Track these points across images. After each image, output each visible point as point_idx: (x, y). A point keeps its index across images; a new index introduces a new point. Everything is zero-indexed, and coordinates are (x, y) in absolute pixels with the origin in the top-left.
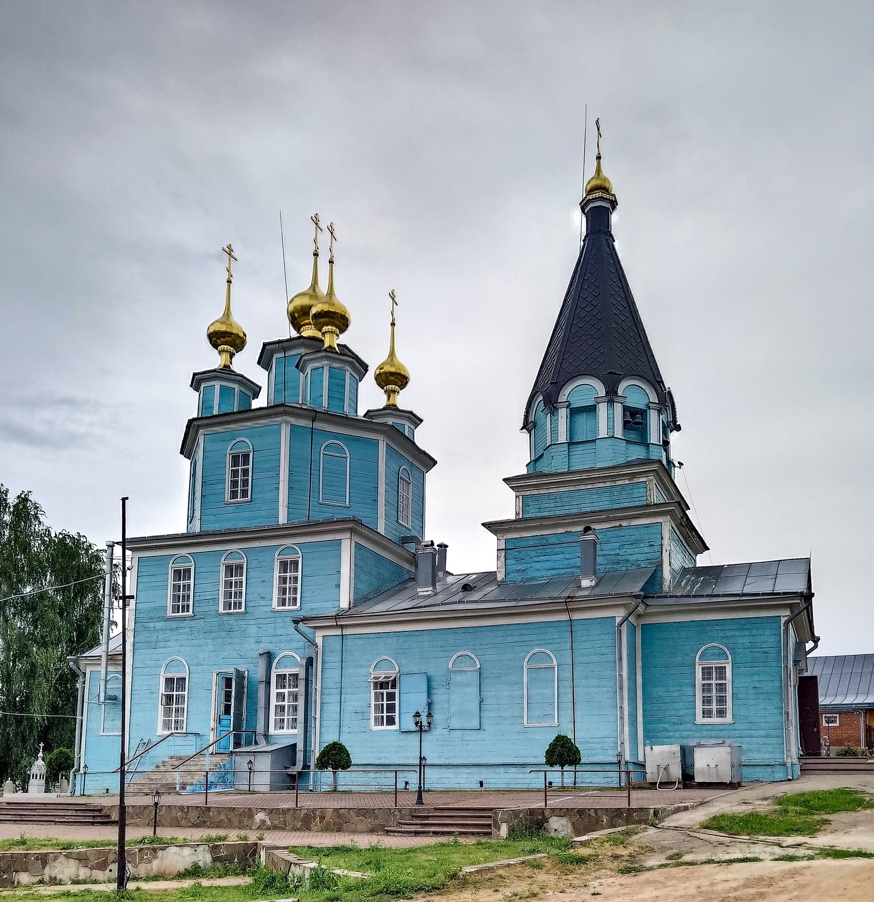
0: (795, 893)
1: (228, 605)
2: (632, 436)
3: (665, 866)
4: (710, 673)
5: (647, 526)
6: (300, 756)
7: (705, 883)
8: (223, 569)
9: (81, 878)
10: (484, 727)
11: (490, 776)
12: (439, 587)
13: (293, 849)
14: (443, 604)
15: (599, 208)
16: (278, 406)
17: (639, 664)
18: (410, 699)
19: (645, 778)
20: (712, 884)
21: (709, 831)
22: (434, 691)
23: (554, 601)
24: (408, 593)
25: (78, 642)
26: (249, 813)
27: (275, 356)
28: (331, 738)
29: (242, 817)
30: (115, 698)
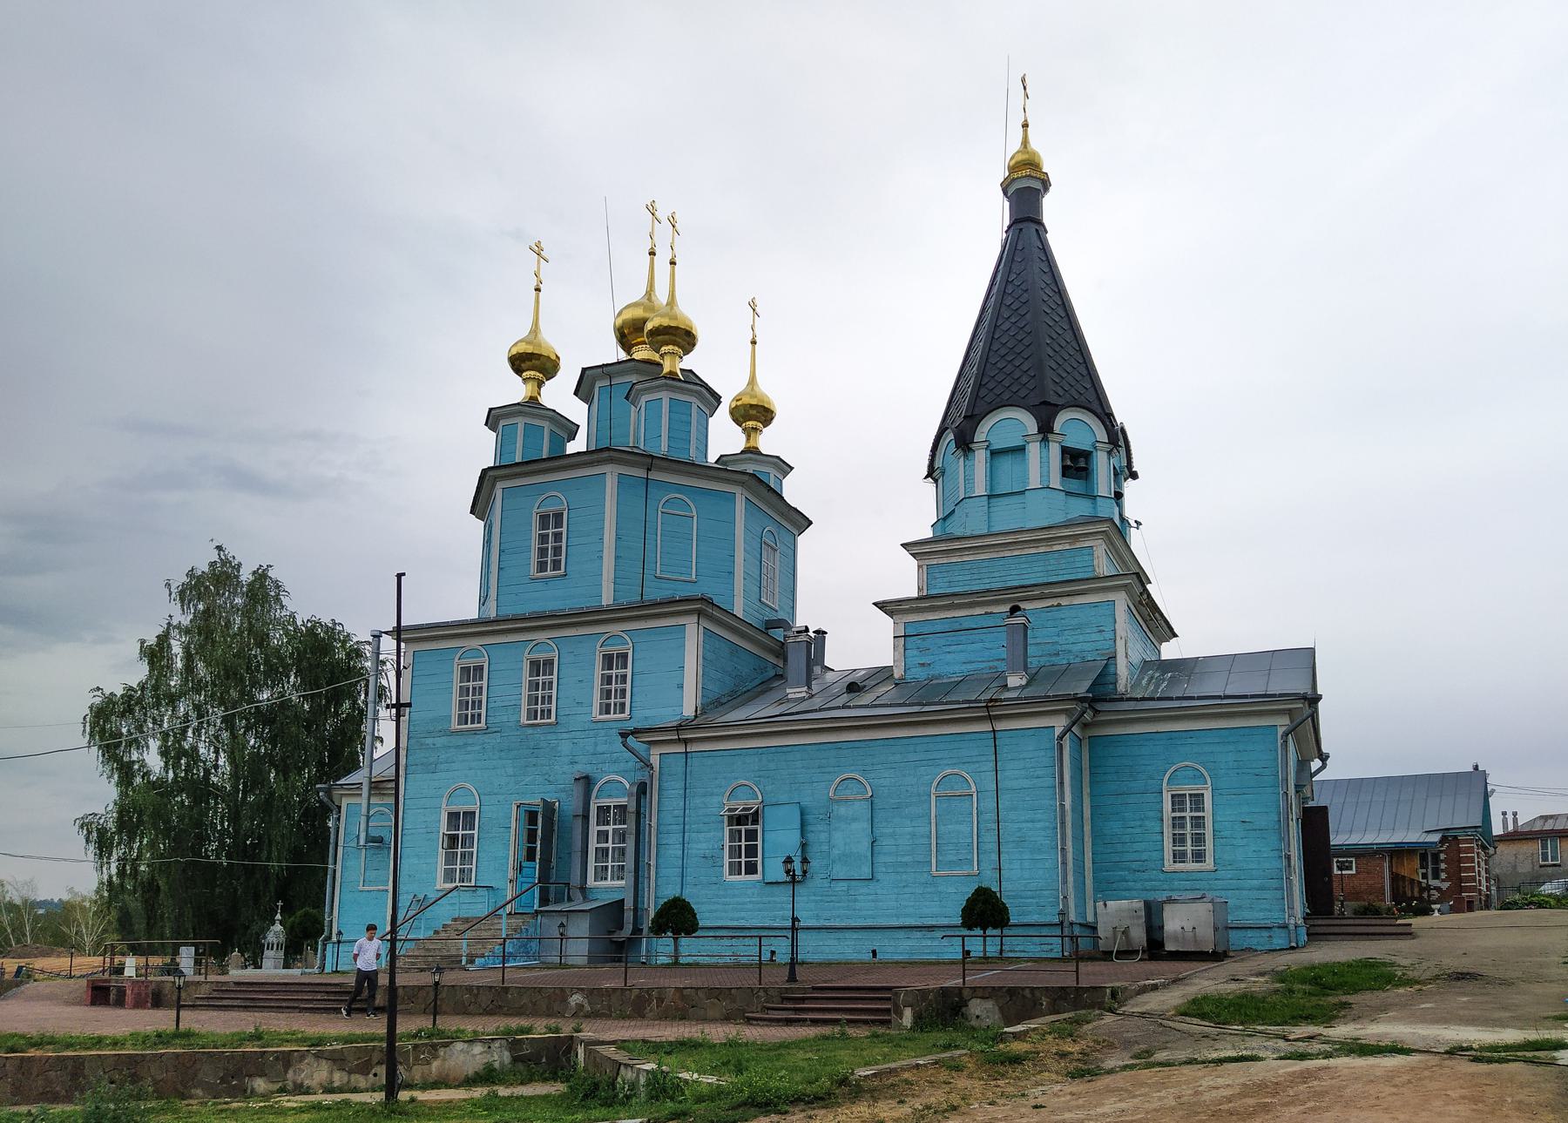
0: (1311, 1104)
1: (533, 714)
2: (1075, 485)
3: (1131, 1067)
4: (1183, 802)
5: (1095, 605)
6: (629, 916)
7: (1187, 1092)
8: (526, 667)
9: (336, 1085)
10: (878, 876)
11: (886, 942)
12: (815, 688)
13: (621, 1045)
14: (820, 710)
15: (1026, 190)
16: (601, 450)
17: (1086, 791)
18: (779, 839)
19: (1096, 945)
20: (1196, 1093)
21: (1188, 1019)
22: (810, 828)
23: (971, 705)
24: (776, 695)
25: (330, 765)
26: (562, 995)
27: (598, 384)
28: (670, 892)
29: (550, 1002)
30: (380, 840)
